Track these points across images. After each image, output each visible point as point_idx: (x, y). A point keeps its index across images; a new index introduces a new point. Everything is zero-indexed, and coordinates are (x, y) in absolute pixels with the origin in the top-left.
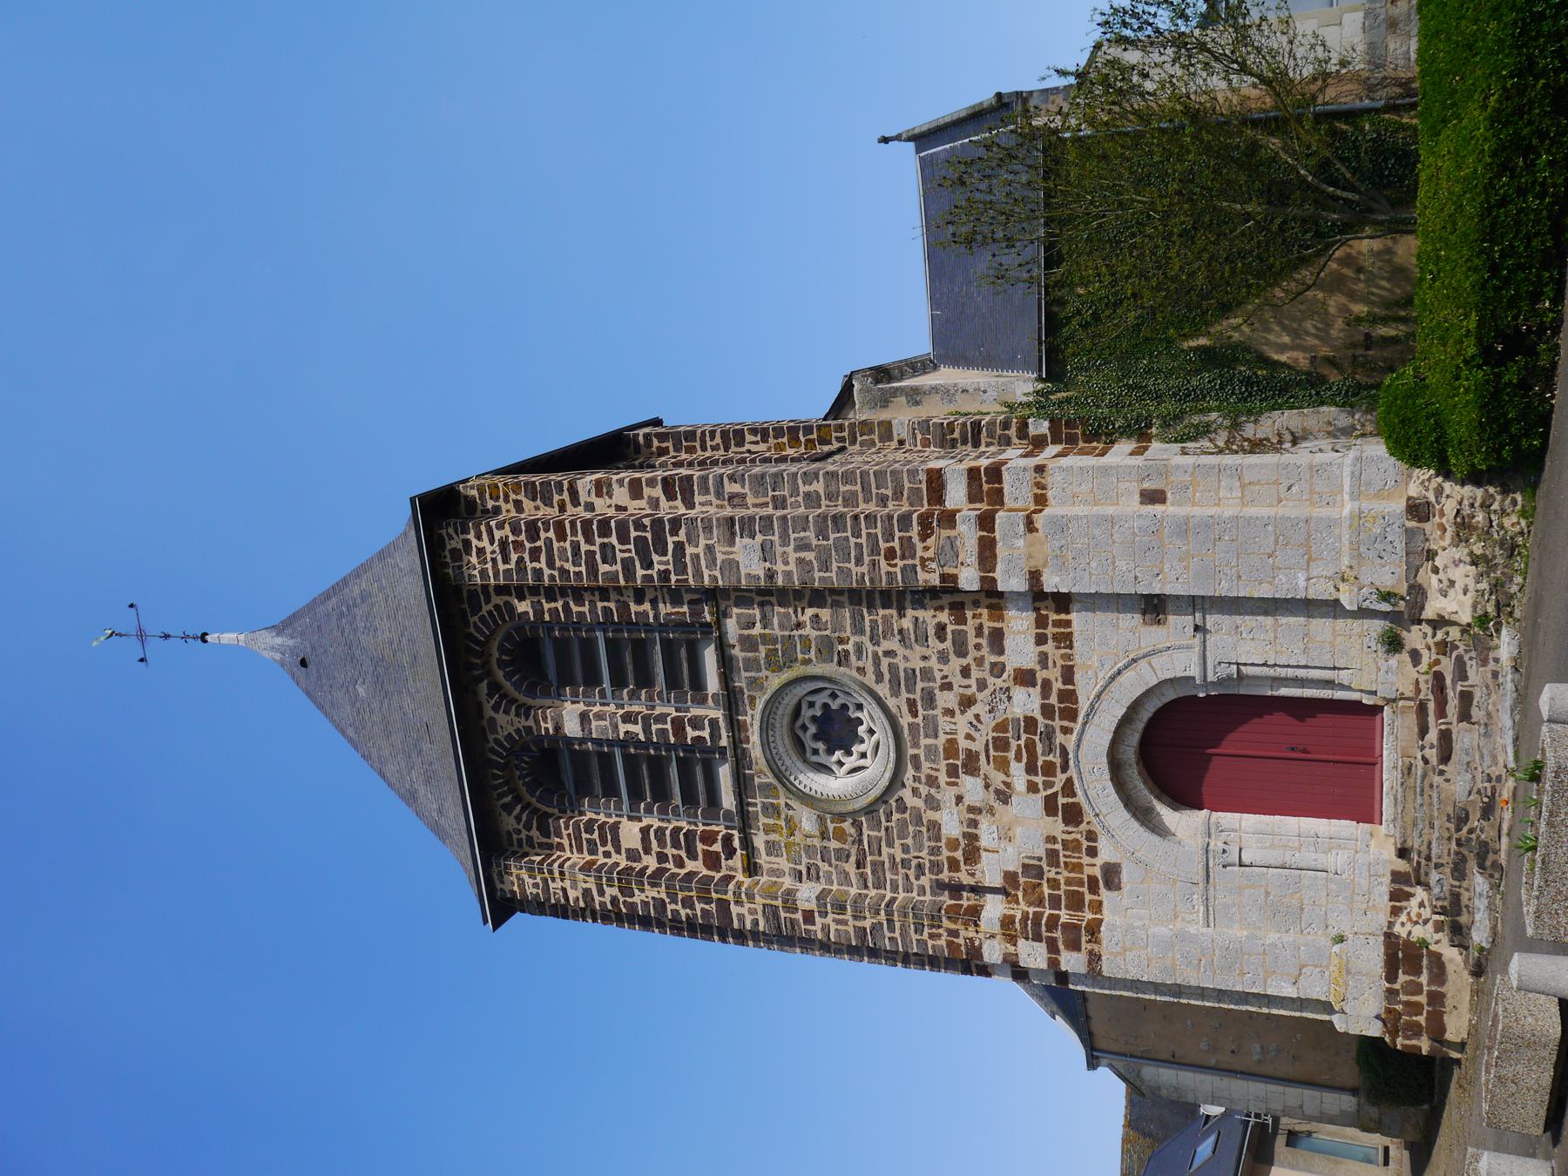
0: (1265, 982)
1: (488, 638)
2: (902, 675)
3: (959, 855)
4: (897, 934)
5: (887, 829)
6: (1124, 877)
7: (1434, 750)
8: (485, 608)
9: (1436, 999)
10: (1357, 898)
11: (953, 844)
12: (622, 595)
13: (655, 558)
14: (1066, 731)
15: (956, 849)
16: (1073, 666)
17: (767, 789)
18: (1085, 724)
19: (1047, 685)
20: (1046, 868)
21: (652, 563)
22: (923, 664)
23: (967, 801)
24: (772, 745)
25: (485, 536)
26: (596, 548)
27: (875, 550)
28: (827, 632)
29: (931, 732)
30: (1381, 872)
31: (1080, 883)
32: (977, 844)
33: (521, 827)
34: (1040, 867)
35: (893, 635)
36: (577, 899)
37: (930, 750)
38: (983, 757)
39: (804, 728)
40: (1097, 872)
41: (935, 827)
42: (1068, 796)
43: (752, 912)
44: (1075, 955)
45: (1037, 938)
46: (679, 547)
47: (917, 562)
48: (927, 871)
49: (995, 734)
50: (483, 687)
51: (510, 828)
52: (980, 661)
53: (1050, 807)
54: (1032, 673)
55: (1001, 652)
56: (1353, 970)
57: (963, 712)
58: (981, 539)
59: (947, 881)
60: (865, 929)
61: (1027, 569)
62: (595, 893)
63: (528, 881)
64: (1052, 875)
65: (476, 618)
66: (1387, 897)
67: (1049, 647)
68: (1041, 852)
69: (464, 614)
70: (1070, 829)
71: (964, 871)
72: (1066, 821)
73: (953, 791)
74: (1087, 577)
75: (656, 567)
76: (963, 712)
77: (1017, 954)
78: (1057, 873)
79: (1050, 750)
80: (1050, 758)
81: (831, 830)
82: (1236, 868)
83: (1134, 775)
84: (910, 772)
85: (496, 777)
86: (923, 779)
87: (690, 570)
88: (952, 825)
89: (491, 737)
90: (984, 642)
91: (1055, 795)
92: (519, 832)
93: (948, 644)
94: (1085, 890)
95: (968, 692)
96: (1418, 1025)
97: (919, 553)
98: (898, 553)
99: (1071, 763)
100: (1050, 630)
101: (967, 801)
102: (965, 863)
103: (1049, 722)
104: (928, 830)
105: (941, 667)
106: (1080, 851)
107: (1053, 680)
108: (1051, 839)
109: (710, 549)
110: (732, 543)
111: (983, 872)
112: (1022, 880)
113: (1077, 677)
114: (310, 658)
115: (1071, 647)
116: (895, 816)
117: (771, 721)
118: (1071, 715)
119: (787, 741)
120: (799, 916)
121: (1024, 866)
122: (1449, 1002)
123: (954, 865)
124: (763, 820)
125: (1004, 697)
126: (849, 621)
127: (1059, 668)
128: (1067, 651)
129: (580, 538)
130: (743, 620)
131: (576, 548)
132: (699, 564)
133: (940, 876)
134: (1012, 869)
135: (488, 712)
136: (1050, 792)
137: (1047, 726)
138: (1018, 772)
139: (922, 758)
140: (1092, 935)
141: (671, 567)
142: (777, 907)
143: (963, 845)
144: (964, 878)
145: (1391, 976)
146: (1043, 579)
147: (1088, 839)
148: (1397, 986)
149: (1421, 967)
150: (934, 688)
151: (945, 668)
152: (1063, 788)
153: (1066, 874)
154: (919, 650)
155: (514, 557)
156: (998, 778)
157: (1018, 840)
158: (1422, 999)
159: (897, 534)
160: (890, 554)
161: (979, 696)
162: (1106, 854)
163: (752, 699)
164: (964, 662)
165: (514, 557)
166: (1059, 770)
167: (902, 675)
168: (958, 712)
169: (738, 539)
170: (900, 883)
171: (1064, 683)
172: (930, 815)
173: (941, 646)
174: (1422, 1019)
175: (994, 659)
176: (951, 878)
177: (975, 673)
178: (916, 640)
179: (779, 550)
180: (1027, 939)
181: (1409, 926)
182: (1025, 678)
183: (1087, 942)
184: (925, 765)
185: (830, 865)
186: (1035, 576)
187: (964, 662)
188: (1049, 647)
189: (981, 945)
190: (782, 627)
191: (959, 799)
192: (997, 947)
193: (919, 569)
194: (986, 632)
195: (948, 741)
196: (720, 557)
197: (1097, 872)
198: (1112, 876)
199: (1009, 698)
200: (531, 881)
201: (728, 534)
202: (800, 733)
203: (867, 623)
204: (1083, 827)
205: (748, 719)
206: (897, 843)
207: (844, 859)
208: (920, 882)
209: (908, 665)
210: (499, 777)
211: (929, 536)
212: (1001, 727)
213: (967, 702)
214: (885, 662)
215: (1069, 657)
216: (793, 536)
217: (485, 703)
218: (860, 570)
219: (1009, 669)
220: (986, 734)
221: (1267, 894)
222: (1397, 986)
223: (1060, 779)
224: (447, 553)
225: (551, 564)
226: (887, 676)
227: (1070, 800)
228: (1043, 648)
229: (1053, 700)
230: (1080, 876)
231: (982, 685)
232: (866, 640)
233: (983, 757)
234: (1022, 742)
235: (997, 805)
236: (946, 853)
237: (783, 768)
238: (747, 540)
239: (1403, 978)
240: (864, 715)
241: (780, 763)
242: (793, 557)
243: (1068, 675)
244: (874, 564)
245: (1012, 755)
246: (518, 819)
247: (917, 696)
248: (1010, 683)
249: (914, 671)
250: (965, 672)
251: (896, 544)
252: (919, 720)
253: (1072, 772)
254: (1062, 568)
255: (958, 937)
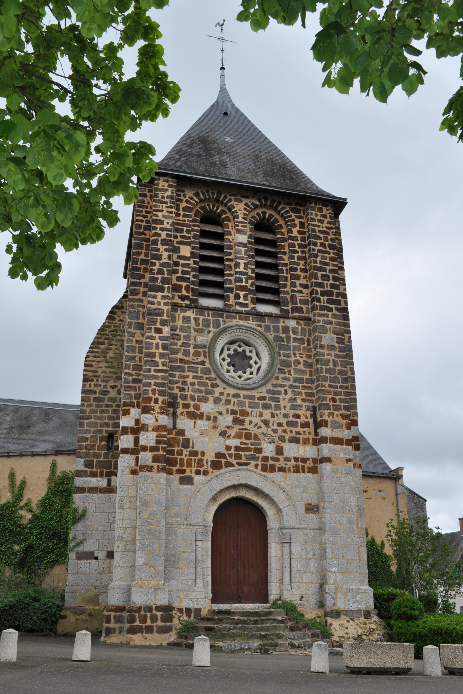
0: (144, 550)
1: (279, 213)
2: (277, 396)
3: (191, 409)
4: (153, 373)
5: (202, 377)
6: (186, 487)
7: (375, 618)
8: (293, 215)
9: (150, 630)
10: (185, 593)
11: (197, 407)
12: (304, 278)
13: (325, 298)
14: (256, 466)
15: (194, 408)
16: (286, 472)
17: (217, 325)
18: (260, 474)
19: (277, 460)
20: (188, 450)
21: (323, 296)
22: (282, 406)
23: (219, 417)
24: (238, 330)
25: (329, 225)
26: (327, 273)
27: (336, 394)
28: (293, 366)
29: (251, 405)
30: (199, 604)
31: (182, 465)
32: (198, 418)
33: (187, 198)
34: (188, 447)
35: (294, 395)
36: (157, 216)
37: (242, 404)
38: (241, 427)
39: (240, 346)
40: (188, 474)
41: (205, 400)
42: (225, 464)
43: (159, 303)
44: (150, 460)
45: (158, 442)
46: (330, 310)
47: (332, 411)
48: (182, 393)
49: (253, 434)
50: (257, 202)
51: (186, 193)
52: (285, 431)
53: (219, 455)
54: (282, 454)
55: (290, 441)
56: (157, 591)
57: (262, 421)
58: (343, 439)
59: (178, 401)
60: (155, 358)
61: (332, 457)
62: (162, 226)
63: (166, 195)
64: (185, 452)
65: (288, 209)
66: (187, 606)
67: (293, 463)
68: (196, 449)
69: (290, 204)
70: (209, 463)
71: (183, 410)
72: (213, 462)
73: (224, 412)
74: (330, 482)
75: (322, 298)
76: (262, 421)
77: (148, 431)
78: (186, 455)
79: (247, 458)
80: (243, 458)
81: (200, 350)
82: (194, 539)
83: (232, 494)
84: (233, 391)
85: (213, 194)
86: (228, 398)
87: (321, 312)
88: (206, 408)
89: (232, 198)
90: (294, 434)
91: (226, 458)
92: (185, 197)
93: (292, 419)
94: (178, 467)
95: (271, 424)
96: (134, 621)
97: (336, 413)
98: (335, 404)
99: (242, 467)
100: (300, 464)
101: (219, 417)
102: (187, 412)
103: (260, 459)
104: (203, 396)
105: (282, 414)
106: (197, 467)
107: (279, 463)
108: (203, 454)
109: (331, 323)
110: (334, 333)
111: (183, 419)
112: (181, 438)
113: (281, 473)
114: (227, 118)
115: (294, 472)
116: (209, 383)
117: (249, 332)
118: (264, 469)
119: (237, 337)
120: (158, 326)
121: (188, 440)
122: (149, 636)
123: (186, 406)
124: (201, 318)
125: (270, 440)
126: (299, 376)
127: (285, 466)
128: (292, 470)
129: (331, 267)
130: (296, 330)
131: (327, 264)
132: (325, 317)
133: (179, 399)
134: (186, 433)
135: (245, 201)
136: (227, 456)
137: (258, 458)
138: (235, 442)
139: (239, 399)
140: (162, 469)
141: (322, 304)
142: (162, 316)
143: (196, 412)
144: (180, 410)
145: (159, 608)
146: (328, 463)
147: (204, 471)
148: (154, 612)
149: (165, 622)
150: (272, 409)
151: (281, 416)
152: (229, 462)
153: (186, 459)
154: (288, 405)
155: (321, 236)
156: (232, 432)
157: (201, 439)
158: (149, 623)
159: (342, 404)
160: (334, 400)
161: (270, 429)
162: (198, 479)
163: (260, 326)
164: (284, 424)
165: (321, 236)
166: (238, 461)
167: (277, 396)
168: (262, 418)
169: (335, 336)
170: (174, 379)
171: (278, 467)
172: (211, 398)
173: (291, 415)
174: (137, 623)
175: (287, 438)
176: (179, 403)
177: (280, 429)
178: (292, 405)
179: (333, 353)
180: (157, 437)
181: (176, 616)
182: (279, 451)
183: (158, 466)
184: (236, 400)
185: (181, 346)
186: (328, 460)
187: (284, 424)
188: (293, 463)
189: (151, 414)
190: (294, 347)
191: (221, 413)
192: (151, 422)
193: (329, 411)
194: (298, 436)
195: (248, 413)
196: (328, 326)
197: (188, 474)
198: (188, 481)
199: (270, 443)
200: (165, 196)
201: (337, 332)
202: (237, 344)
203: (298, 385)
204: (210, 470)
205: (251, 322)
206: (196, 381)
207: (185, 353)
208: (175, 389)
209: (281, 400)
210: (213, 195)
211: (342, 418)
212: (256, 437)
213: (266, 423)
214: (282, 389)
215: (289, 471)
216: (339, 360)
217: (249, 200)
218: (327, 386)
219: (283, 444)
220: (253, 430)
221: (184, 552)
222: (154, 612)
223: (234, 461)
224: (321, 206)
225: (319, 251)
226: (276, 389)
227: (223, 465)
228: (293, 460)
229: (271, 462)
230: (185, 465)
231: (275, 431)
232: (291, 383)
233: (241, 427)
234: (250, 446)
235: (218, 431)
236: (192, 403)
237: (227, 333)
238: (335, 340)
239: (159, 614)
240: (235, 375)
241: (229, 332)
242: (331, 358)
243: (282, 470)
244: (329, 392)
245: (244, 440)
246: (191, 198)
247: (267, 401)
248: (277, 444)
249: (279, 402)
250: (280, 425)
251: (338, 403)
252: (256, 401)
253: (237, 467)
254: (334, 471)
255: (155, 403)
